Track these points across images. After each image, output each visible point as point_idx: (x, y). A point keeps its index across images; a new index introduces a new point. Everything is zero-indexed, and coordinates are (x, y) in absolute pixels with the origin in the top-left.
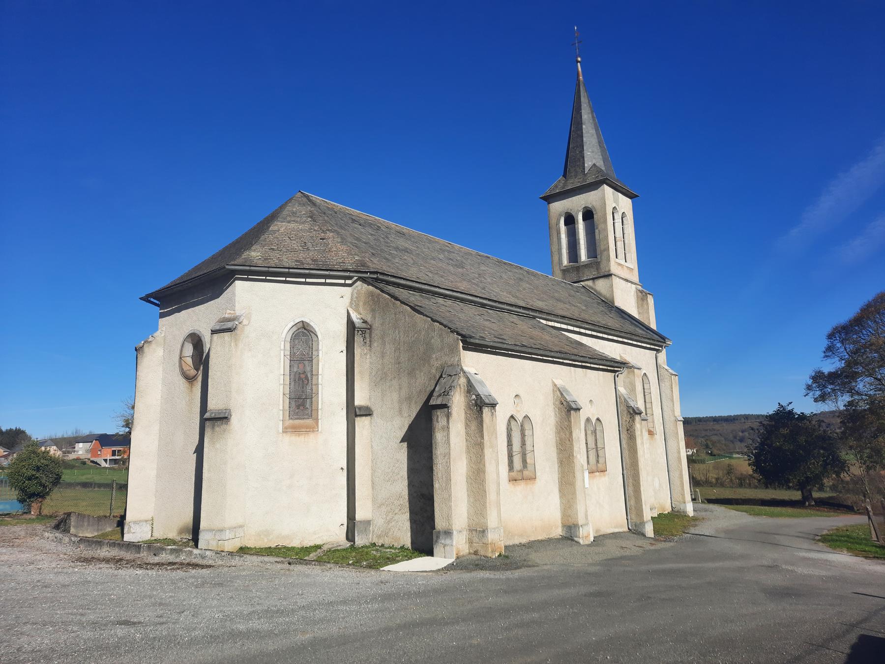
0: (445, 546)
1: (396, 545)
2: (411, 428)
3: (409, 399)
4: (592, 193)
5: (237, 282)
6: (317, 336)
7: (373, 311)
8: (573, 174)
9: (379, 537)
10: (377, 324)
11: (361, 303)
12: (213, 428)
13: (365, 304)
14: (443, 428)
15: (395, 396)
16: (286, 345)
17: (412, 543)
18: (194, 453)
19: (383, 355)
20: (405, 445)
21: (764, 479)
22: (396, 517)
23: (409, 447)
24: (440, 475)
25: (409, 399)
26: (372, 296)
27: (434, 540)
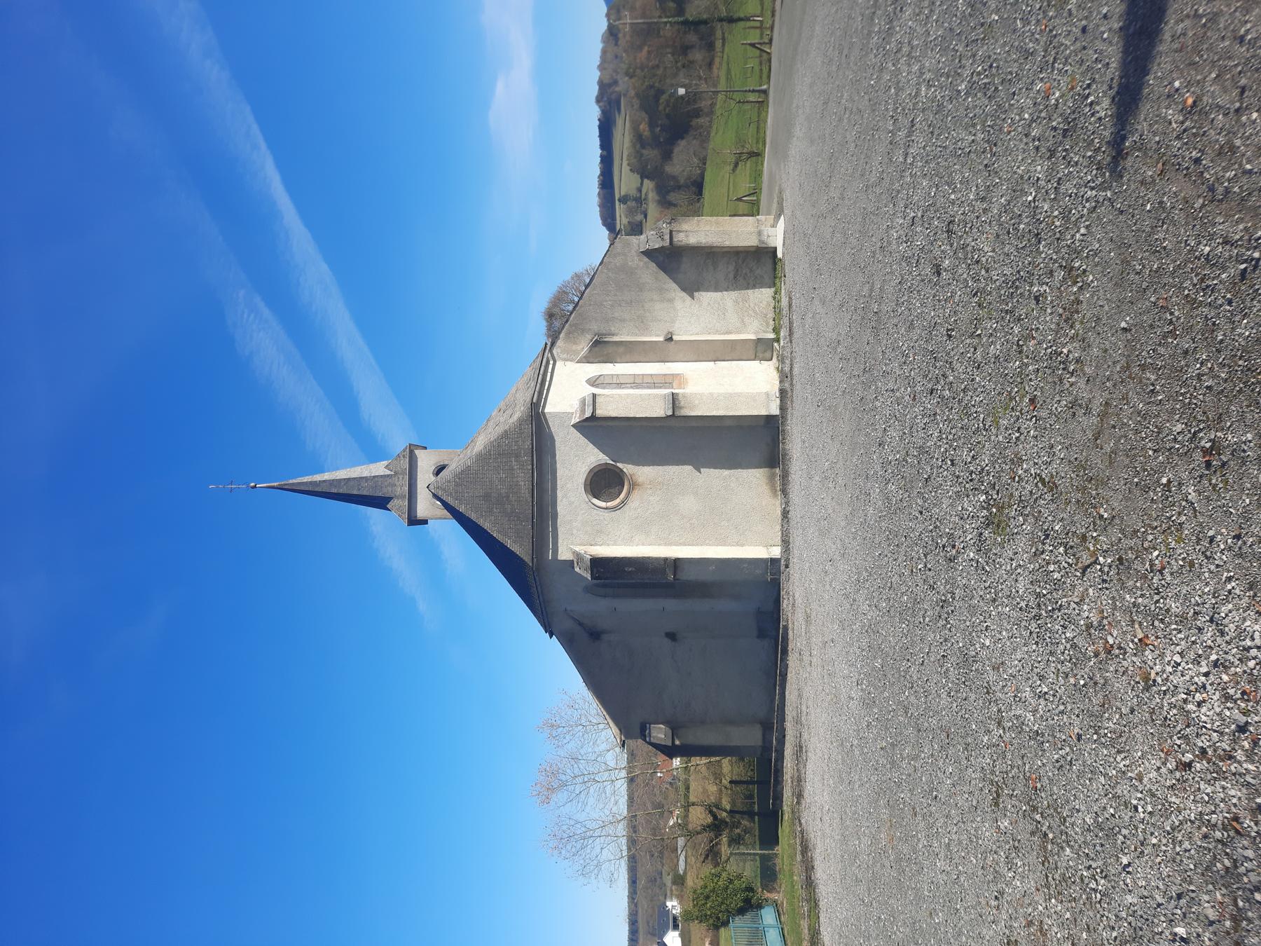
0: (769, 236)
1: (772, 305)
2: (684, 289)
3: (661, 290)
4: (419, 464)
5: (546, 411)
6: (600, 376)
7: (583, 331)
8: (390, 489)
9: (767, 324)
10: (595, 327)
11: (574, 347)
12: (681, 408)
13: (575, 343)
14: (687, 236)
15: (658, 306)
16: (594, 502)
17: (770, 287)
18: (700, 473)
19: (623, 320)
20: (696, 294)
21: (734, 758)
22: (752, 305)
23: (698, 290)
24: (720, 240)
25: (661, 290)
26: (569, 333)
27: (766, 246)
